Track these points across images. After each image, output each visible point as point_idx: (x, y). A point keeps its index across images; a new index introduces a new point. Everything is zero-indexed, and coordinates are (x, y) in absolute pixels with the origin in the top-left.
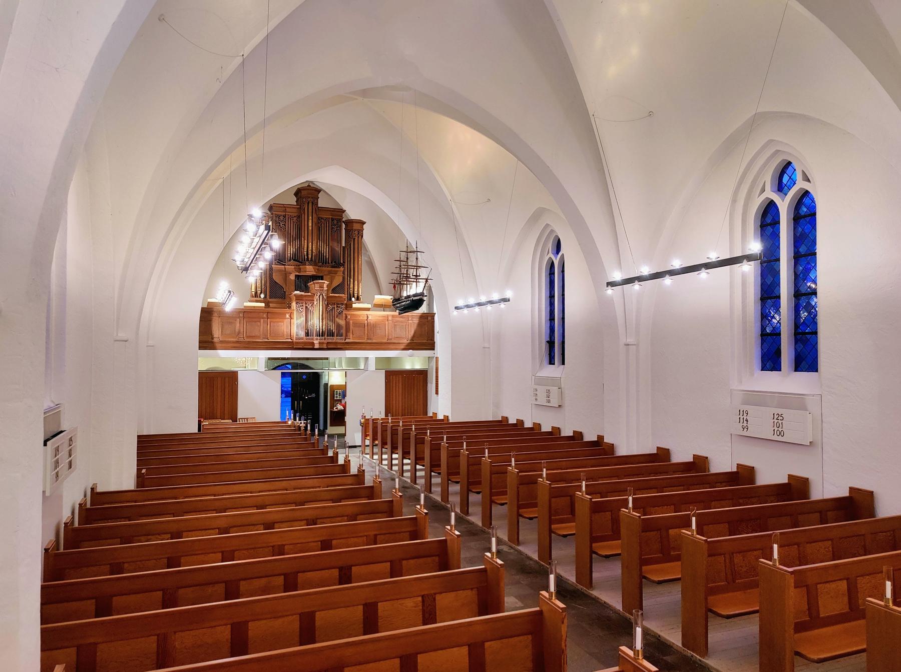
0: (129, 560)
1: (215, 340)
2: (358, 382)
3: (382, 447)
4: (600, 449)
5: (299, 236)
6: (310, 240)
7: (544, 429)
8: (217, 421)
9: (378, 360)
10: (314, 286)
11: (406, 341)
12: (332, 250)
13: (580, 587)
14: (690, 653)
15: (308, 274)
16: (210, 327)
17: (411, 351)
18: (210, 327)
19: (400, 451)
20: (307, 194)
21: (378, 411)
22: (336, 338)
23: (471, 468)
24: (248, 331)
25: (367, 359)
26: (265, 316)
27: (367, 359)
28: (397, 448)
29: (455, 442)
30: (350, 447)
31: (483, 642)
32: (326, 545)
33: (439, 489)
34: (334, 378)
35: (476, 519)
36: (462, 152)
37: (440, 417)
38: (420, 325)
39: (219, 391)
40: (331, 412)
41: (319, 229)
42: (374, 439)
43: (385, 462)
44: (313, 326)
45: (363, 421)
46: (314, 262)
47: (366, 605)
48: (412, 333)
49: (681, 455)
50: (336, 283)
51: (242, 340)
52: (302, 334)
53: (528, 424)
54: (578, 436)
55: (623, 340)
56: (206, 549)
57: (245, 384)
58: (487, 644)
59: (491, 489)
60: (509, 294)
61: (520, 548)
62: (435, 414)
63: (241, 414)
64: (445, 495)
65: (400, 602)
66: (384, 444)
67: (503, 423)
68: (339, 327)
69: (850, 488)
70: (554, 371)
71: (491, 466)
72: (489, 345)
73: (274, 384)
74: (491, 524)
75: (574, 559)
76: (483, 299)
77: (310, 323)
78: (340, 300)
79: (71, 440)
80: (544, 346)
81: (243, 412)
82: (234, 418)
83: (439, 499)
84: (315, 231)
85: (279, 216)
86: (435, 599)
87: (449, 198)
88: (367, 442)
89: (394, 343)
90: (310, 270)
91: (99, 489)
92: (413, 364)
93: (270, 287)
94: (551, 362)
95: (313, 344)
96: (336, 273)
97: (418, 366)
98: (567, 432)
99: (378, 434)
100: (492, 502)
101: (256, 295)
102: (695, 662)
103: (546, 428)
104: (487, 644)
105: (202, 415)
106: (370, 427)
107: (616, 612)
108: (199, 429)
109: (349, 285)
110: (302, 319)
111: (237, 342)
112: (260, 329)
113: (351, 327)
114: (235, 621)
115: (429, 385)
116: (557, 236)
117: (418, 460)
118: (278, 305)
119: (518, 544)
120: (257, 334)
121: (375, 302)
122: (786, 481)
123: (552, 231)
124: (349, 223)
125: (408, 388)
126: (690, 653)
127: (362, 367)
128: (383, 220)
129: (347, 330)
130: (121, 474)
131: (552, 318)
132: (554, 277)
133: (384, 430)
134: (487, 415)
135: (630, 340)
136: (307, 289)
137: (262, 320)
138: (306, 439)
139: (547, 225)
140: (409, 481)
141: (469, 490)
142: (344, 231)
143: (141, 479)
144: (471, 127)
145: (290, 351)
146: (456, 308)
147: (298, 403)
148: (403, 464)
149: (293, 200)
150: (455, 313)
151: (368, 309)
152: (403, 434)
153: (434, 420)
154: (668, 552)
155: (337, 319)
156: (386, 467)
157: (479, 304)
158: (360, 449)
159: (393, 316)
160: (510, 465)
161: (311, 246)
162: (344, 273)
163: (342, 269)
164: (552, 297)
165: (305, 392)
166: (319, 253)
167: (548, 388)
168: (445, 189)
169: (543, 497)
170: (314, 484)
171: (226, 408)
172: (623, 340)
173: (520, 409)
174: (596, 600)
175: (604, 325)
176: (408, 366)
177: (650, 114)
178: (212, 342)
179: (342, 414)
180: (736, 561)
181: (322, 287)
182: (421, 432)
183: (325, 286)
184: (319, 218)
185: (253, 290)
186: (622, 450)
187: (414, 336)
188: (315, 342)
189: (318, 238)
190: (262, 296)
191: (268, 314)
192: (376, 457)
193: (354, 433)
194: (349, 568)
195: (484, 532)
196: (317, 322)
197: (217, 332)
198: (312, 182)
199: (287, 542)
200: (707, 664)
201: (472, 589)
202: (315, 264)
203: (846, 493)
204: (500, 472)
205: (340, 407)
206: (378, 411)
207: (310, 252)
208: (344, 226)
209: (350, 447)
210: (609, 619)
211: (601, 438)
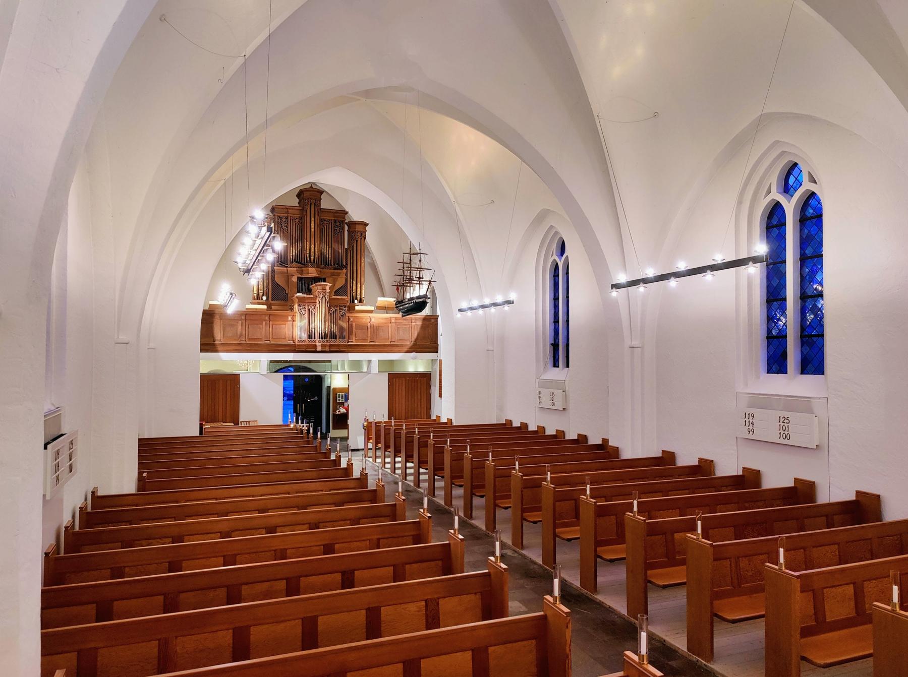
0: (130, 564)
1: (217, 342)
2: (361, 385)
3: (385, 451)
4: (605, 452)
5: (301, 238)
6: (313, 242)
7: (548, 433)
8: (219, 424)
9: (381, 362)
11: (409, 344)
12: (335, 252)
13: (584, 591)
14: (695, 658)
15: (310, 276)
16: (211, 329)
17: (414, 353)
18: (211, 329)
19: (403, 454)
20: (310, 196)
21: (381, 414)
22: (339, 340)
23: (474, 472)
24: (250, 333)
25: (370, 361)
26: (267, 318)
27: (370, 361)
28: (400, 451)
29: (458, 445)
30: (353, 450)
31: (487, 647)
32: (328, 549)
34: (336, 381)
35: (480, 523)
36: (466, 153)
37: (444, 420)
38: (423, 327)
39: (221, 394)
40: (334, 415)
41: (321, 231)
42: (377, 442)
43: (388, 466)
44: (315, 328)
45: (365, 424)
46: (316, 264)
47: (369, 610)
48: (415, 335)
49: (686, 458)
50: (339, 285)
51: (244, 342)
52: (304, 336)
53: (532, 427)
54: (582, 439)
55: (628, 343)
56: (208, 553)
57: (247, 386)
58: (491, 649)
59: (495, 492)
60: (513, 296)
61: (524, 552)
62: (438, 417)
63: (243, 417)
64: (449, 499)
65: (403, 606)
66: (387, 447)
67: (507, 426)
68: (341, 329)
69: (857, 492)
70: (558, 374)
71: (495, 470)
72: (492, 348)
73: (276, 387)
74: (495, 528)
75: (579, 563)
76: (487, 301)
77: (312, 326)
78: (343, 302)
79: (71, 443)
80: (549, 349)
81: (245, 415)
82: (236, 422)
83: (442, 502)
84: (317, 233)
85: (281, 218)
86: (438, 604)
87: (453, 199)
88: (370, 446)
89: (397, 346)
90: (312, 272)
91: (100, 493)
92: (416, 367)
93: (272, 290)
94: (556, 365)
95: (316, 346)
96: (338, 275)
97: (421, 369)
98: (571, 435)
99: (381, 437)
100: (496, 505)
101: (258, 297)
102: (700, 667)
103: (550, 431)
104: (491, 649)
105: (204, 418)
106: (373, 431)
107: (620, 616)
108: (201, 433)
109: (351, 288)
110: (304, 322)
111: (239, 344)
112: (262, 332)
113: (354, 329)
114: (237, 625)
115: (432, 388)
116: (561, 238)
117: (422, 463)
118: (280, 308)
119: (522, 548)
120: (259, 336)
121: (378, 304)
122: (792, 485)
123: (556, 233)
124: (352, 224)
125: (411, 391)
126: (695, 658)
127: (365, 370)
128: (386, 221)
129: (350, 333)
130: (122, 478)
131: (556, 321)
132: (558, 279)
133: (387, 433)
134: (491, 418)
135: (635, 343)
136: (309, 291)
137: (264, 323)
139: (552, 227)
140: (412, 484)
141: (472, 494)
142: (346, 233)
143: (142, 483)
144: (474, 128)
145: (292, 354)
146: (460, 310)
147: (300, 406)
148: (406, 468)
149: (295, 202)
150: (459, 315)
151: (371, 312)
152: (406, 437)
153: (437, 423)
154: (673, 556)
155: (340, 322)
156: (389, 471)
157: (483, 307)
158: (363, 452)
159: (396, 319)
160: (514, 469)
161: (313, 248)
162: (346, 275)
163: (344, 271)
164: (556, 299)
165: (308, 395)
166: (322, 254)
167: (553, 391)
168: (448, 191)
169: (547, 500)
171: (228, 411)
172: (628, 343)
173: (524, 412)
174: (600, 605)
175: (608, 327)
176: (411, 369)
177: (655, 115)
178: (214, 345)
179: (345, 417)
180: (741, 565)
181: (324, 289)
182: (424, 435)
183: (328, 288)
184: (321, 220)
185: (255, 292)
186: (627, 454)
187: (417, 339)
188: (318, 344)
189: (321, 240)
190: (264, 298)
191: (270, 316)
192: (379, 460)
193: (356, 436)
194: (352, 572)
195: (487, 536)
196: (319, 324)
197: (218, 334)
198: (314, 183)
199: (289, 546)
200: (712, 669)
201: (475, 593)
202: (318, 266)
203: (852, 497)
204: (504, 475)
205: (343, 410)
206: (381, 414)
207: (312, 254)
208: (346, 228)
209: (353, 450)
210: (614, 623)
211: (605, 441)
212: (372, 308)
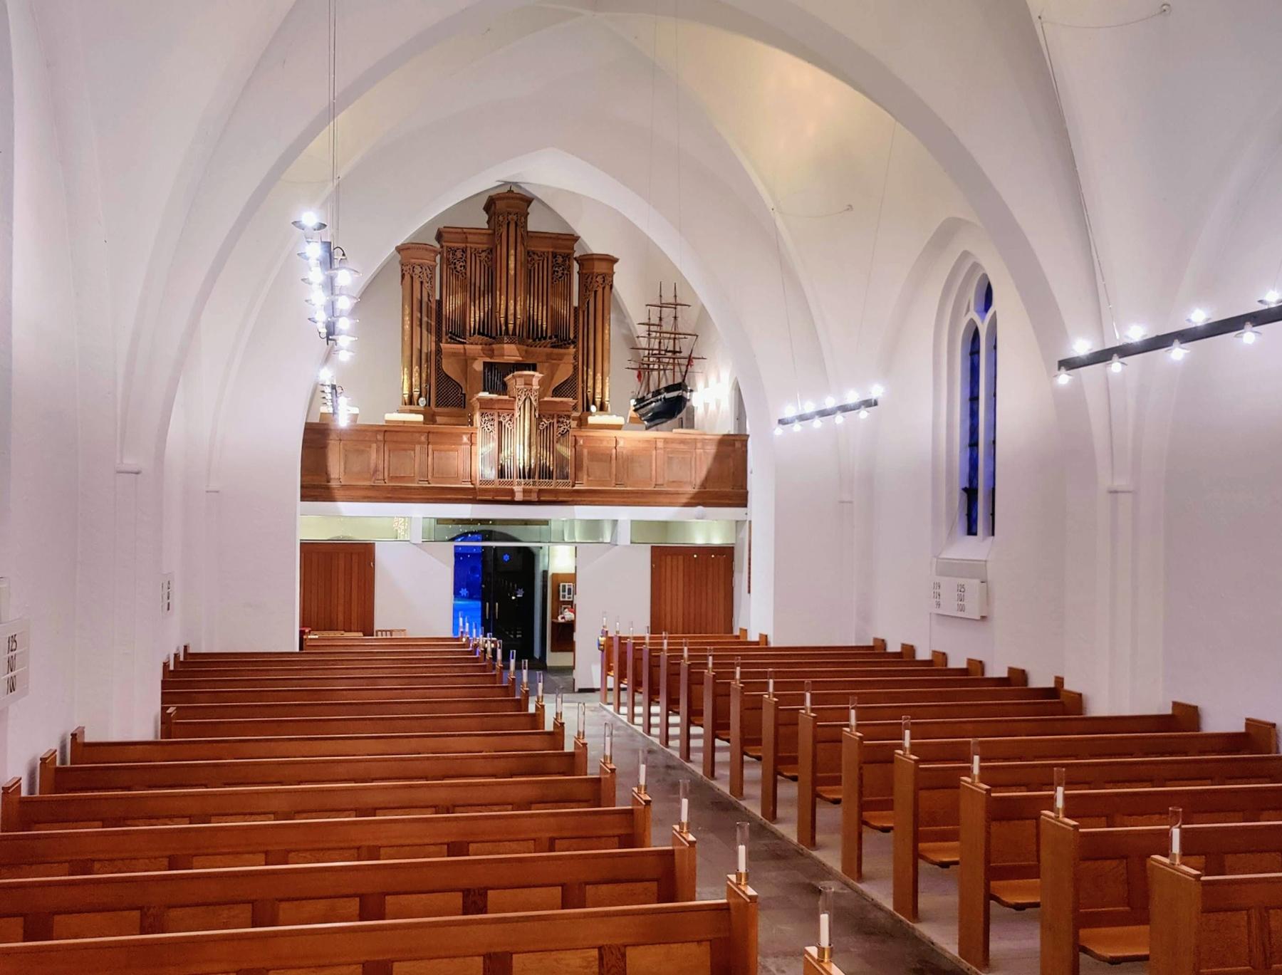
0: (102, 856)
1: (334, 484)
2: (599, 567)
3: (635, 691)
4: (1059, 703)
5: (491, 289)
6: (511, 295)
7: (953, 664)
8: (338, 634)
9: (635, 524)
10: (516, 381)
11: (691, 490)
12: (555, 317)
13: (965, 964)
15: (507, 359)
17: (700, 508)
19: (663, 698)
20: (508, 207)
22: (553, 483)
23: (782, 730)
25: (615, 522)
26: (423, 438)
27: (615, 522)
28: (658, 693)
29: (754, 682)
30: (581, 691)
34: (558, 560)
36: (791, 112)
37: (753, 636)
38: (719, 457)
39: (341, 585)
41: (529, 274)
42: (621, 676)
43: (638, 720)
46: (515, 337)
47: (489, 957)
48: (703, 473)
52: (491, 474)
53: (923, 654)
55: (1105, 481)
56: (243, 844)
59: (814, 771)
61: (862, 887)
62: (744, 631)
63: (378, 625)
64: (738, 784)
65: (555, 955)
66: (637, 684)
67: (877, 651)
68: (561, 461)
71: (815, 727)
72: (851, 498)
73: (439, 572)
74: (813, 838)
77: (505, 453)
78: (567, 405)
80: (958, 499)
82: (368, 629)
83: (725, 789)
85: (453, 251)
86: (624, 955)
87: (770, 204)
88: (611, 682)
89: (667, 493)
90: (510, 352)
94: (971, 531)
95: (512, 492)
96: (560, 358)
97: (717, 540)
98: (996, 670)
99: (634, 668)
100: (816, 795)
101: (411, 402)
103: (957, 661)
106: (619, 655)
108: (301, 648)
109: (585, 382)
110: (496, 446)
112: (414, 464)
113: (586, 462)
114: (245, 966)
115: (736, 575)
116: (985, 276)
118: (453, 420)
119: (860, 877)
123: (976, 266)
124: (588, 260)
125: (695, 581)
127: (608, 539)
128: (650, 254)
129: (578, 466)
130: (133, 716)
131: (973, 444)
132: (976, 355)
134: (842, 633)
135: (1121, 483)
136: (504, 389)
137: (418, 447)
138: (484, 668)
139: (966, 254)
140: (677, 754)
141: (777, 772)
145: (469, 506)
146: (781, 422)
147: (492, 608)
148: (668, 725)
149: (481, 220)
150: (779, 431)
151: (619, 427)
152: (690, 674)
155: (558, 447)
156: (640, 729)
158: (597, 696)
159: (666, 441)
162: (576, 358)
163: (572, 350)
164: (974, 399)
165: (502, 584)
167: (961, 581)
168: (761, 188)
169: (904, 788)
170: (466, 745)
171: (354, 615)
172: (1105, 481)
173: (907, 625)
175: (1069, 452)
176: (699, 539)
178: (328, 488)
179: (570, 626)
180: (1273, 923)
181: (528, 383)
183: (535, 382)
185: (406, 391)
186: (1099, 707)
187: (707, 479)
188: (516, 488)
189: (528, 291)
190: (422, 401)
191: (428, 434)
192: (624, 710)
194: (483, 892)
195: (800, 854)
196: (519, 452)
197: (336, 468)
198: (516, 184)
199: (385, 842)
201: (699, 942)
202: (522, 342)
204: (830, 739)
205: (568, 615)
207: (511, 318)
208: (576, 267)
211: (1060, 681)
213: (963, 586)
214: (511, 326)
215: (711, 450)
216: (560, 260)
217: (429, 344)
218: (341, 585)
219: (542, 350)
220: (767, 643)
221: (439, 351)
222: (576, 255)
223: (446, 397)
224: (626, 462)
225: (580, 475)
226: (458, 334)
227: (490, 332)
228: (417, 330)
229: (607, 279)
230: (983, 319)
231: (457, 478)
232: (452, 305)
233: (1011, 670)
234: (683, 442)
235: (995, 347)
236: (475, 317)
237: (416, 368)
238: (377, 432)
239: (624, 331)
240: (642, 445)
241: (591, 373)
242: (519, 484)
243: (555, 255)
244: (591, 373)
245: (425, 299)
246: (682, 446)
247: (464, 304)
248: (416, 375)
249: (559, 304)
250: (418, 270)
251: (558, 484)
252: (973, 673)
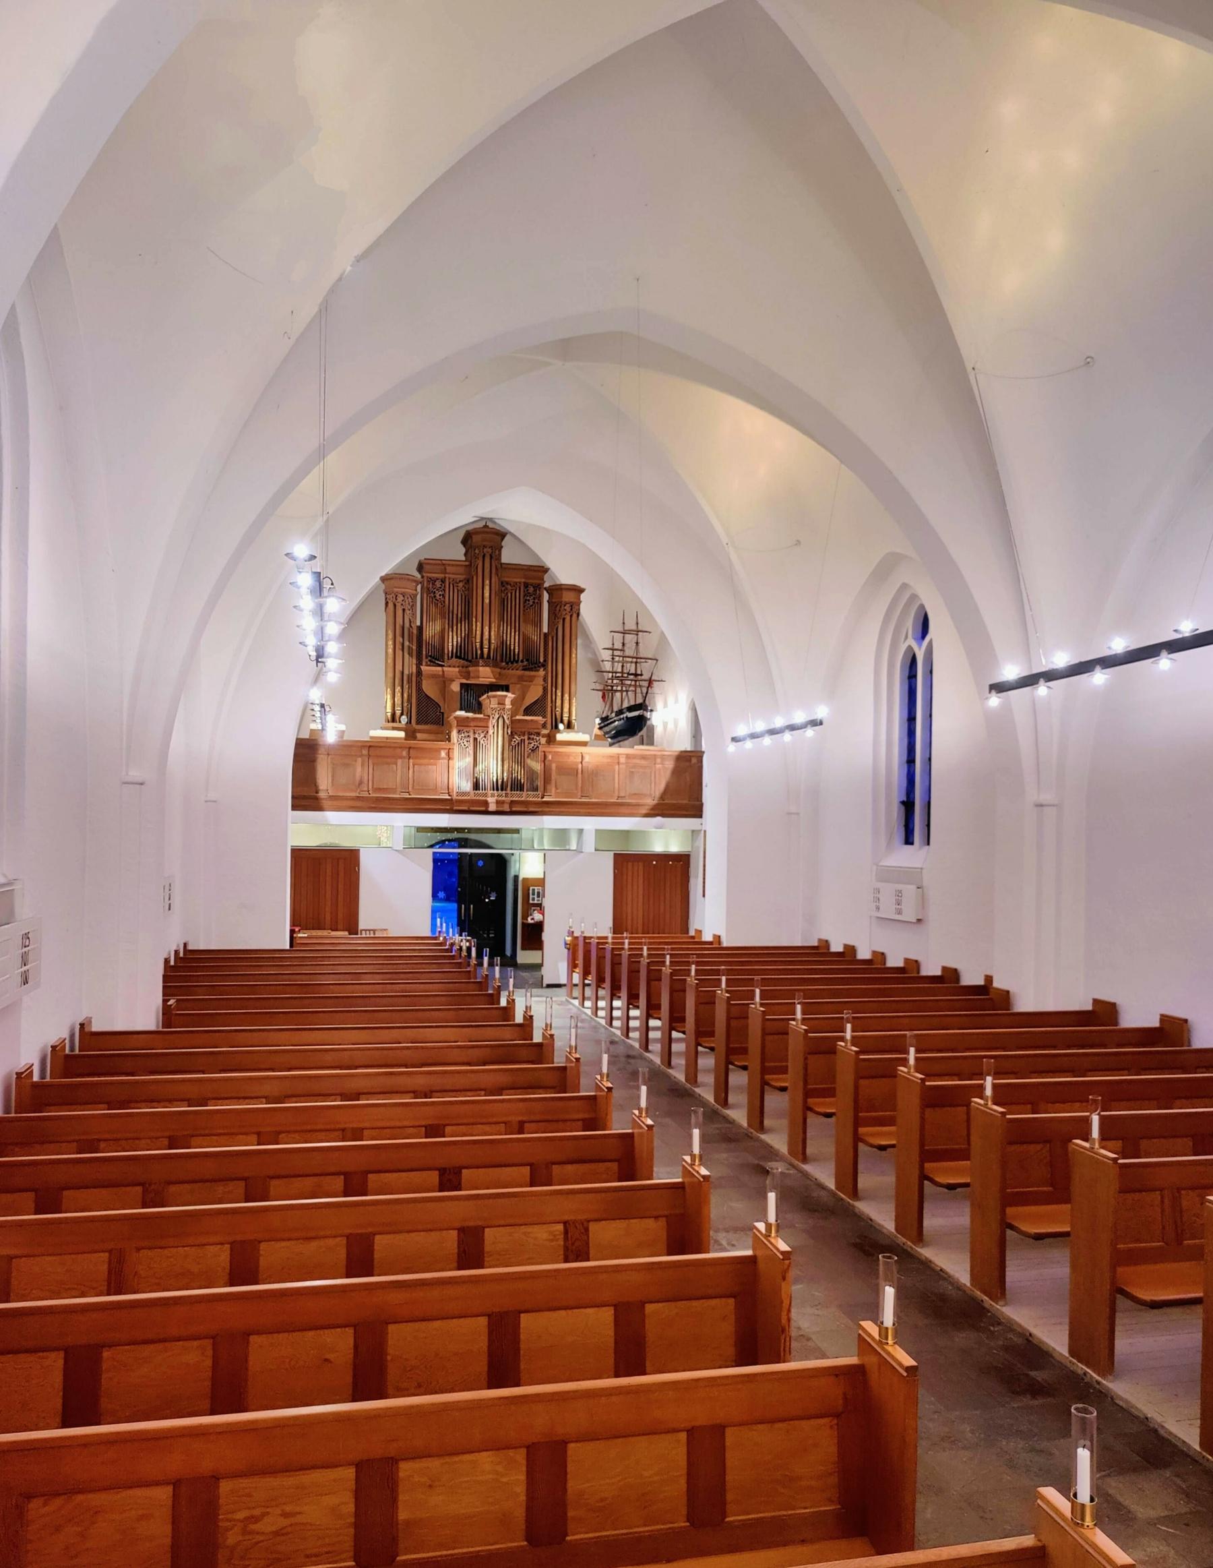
1: (322, 795)
2: (566, 874)
3: (598, 986)
4: (988, 999)
5: (467, 616)
9: (599, 832)
11: (650, 802)
12: (526, 640)
13: (901, 1239)
14: (1081, 1367)
15: (482, 681)
16: (309, 775)
17: (659, 818)
19: (624, 994)
20: (484, 541)
21: (598, 921)
22: (523, 794)
25: (581, 831)
26: (404, 753)
27: (581, 831)
28: (619, 988)
29: (708, 978)
30: (549, 986)
31: (642, 1304)
32: (433, 1130)
33: (683, 1062)
35: (739, 1116)
36: (745, 455)
38: (676, 772)
39: (328, 888)
40: (523, 924)
41: (503, 602)
42: (586, 973)
43: (601, 1013)
44: (487, 770)
45: (569, 939)
46: (491, 661)
48: (662, 786)
49: (1138, 1014)
50: (531, 698)
51: (365, 794)
52: (467, 786)
53: (864, 954)
54: (951, 975)
57: (370, 867)
58: (649, 1308)
60: (822, 712)
61: (807, 1167)
62: (699, 932)
64: (692, 1073)
66: (600, 981)
68: (532, 774)
69: (1162, 1015)
72: (797, 811)
74: (762, 1122)
75: (893, 1193)
76: (779, 722)
77: (480, 767)
78: (536, 723)
79: (26, 936)
80: (896, 812)
81: (368, 918)
82: (353, 928)
85: (433, 581)
86: (587, 1230)
87: (725, 540)
88: (576, 978)
89: (628, 805)
90: (485, 674)
91: (95, 1027)
93: (418, 705)
94: (909, 840)
95: (486, 803)
96: (531, 679)
97: (674, 848)
98: (931, 968)
99: (598, 965)
100: (764, 1083)
102: (1089, 1385)
103: (895, 961)
104: (649, 1308)
105: (298, 921)
107: (959, 1287)
108: (291, 945)
109: (554, 702)
110: (471, 760)
112: (397, 777)
114: (239, 1238)
116: (922, 607)
117: (652, 1010)
119: (805, 1159)
122: (1157, 1024)
123: (914, 597)
124: (556, 590)
125: (652, 886)
126: (1081, 1367)
127: (574, 847)
128: (612, 582)
129: (547, 779)
131: (911, 761)
132: (914, 679)
133: (616, 964)
135: (1046, 797)
136: (479, 708)
137: (399, 762)
139: (905, 586)
140: (637, 1045)
143: (167, 1014)
144: (762, 408)
146: (734, 739)
147: (467, 909)
148: (628, 1018)
150: (732, 748)
151: (584, 744)
152: (649, 971)
153: (696, 942)
154: (1059, 1185)
155: (529, 761)
156: (603, 1022)
157: (772, 732)
159: (628, 756)
160: (794, 1019)
161: (487, 633)
162: (545, 680)
163: (542, 672)
164: (911, 719)
165: (477, 888)
169: (845, 1078)
173: (851, 927)
174: (926, 1265)
175: (998, 768)
176: (658, 848)
177: (1089, 362)
178: (317, 799)
179: (539, 926)
180: (1185, 1204)
181: (501, 703)
182: (680, 964)
184: (502, 584)
185: (389, 710)
186: (1025, 1003)
190: (404, 719)
191: (409, 749)
193: (554, 960)
195: (749, 1136)
196: (493, 766)
197: (324, 781)
198: (491, 520)
199: (367, 1125)
200: (1108, 1389)
201: (656, 1217)
202: (496, 665)
203: (1155, 1023)
204: (777, 1031)
205: (537, 917)
206: (598, 921)
207: (486, 643)
208: (546, 596)
209: (549, 986)
210: (943, 1298)
211: (989, 979)
212: (585, 737)
213: (900, 892)
214: (486, 651)
215: (670, 765)
216: (531, 590)
217: (410, 666)
218: (328, 888)
219: (515, 672)
220: (720, 943)
221: (419, 673)
222: (546, 585)
223: (426, 716)
224: (590, 776)
225: (548, 787)
226: (437, 657)
227: (467, 656)
228: (399, 653)
229: (575, 608)
230: (920, 645)
231: (435, 790)
232: (432, 630)
233: (944, 969)
234: (644, 757)
235: (931, 672)
236: (453, 641)
237: (398, 689)
238: (363, 747)
239: (590, 655)
240: (605, 760)
241: (559, 694)
242: (493, 796)
243: (526, 585)
244: (559, 694)
245: (407, 625)
246: (643, 762)
247: (443, 631)
248: (398, 695)
249: (530, 630)
250: (400, 598)
251: (528, 796)
252: (909, 971)
